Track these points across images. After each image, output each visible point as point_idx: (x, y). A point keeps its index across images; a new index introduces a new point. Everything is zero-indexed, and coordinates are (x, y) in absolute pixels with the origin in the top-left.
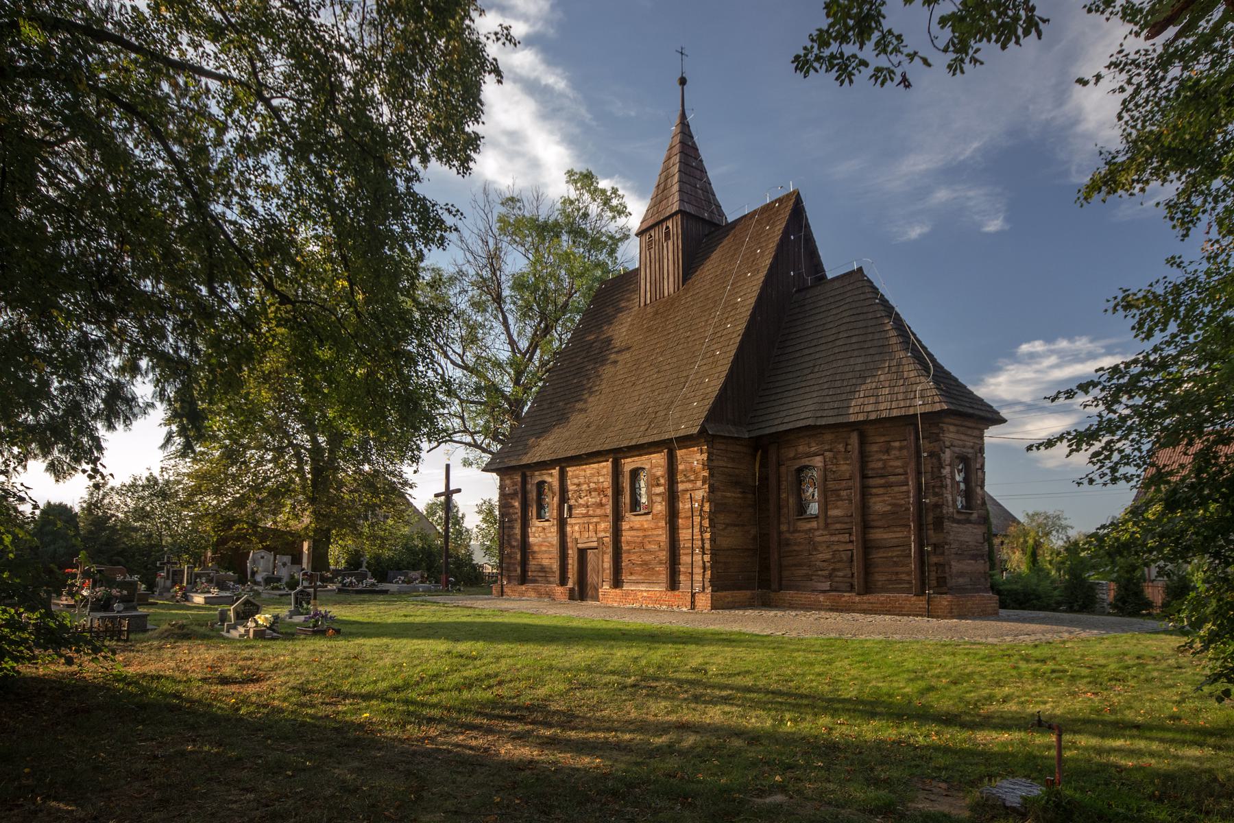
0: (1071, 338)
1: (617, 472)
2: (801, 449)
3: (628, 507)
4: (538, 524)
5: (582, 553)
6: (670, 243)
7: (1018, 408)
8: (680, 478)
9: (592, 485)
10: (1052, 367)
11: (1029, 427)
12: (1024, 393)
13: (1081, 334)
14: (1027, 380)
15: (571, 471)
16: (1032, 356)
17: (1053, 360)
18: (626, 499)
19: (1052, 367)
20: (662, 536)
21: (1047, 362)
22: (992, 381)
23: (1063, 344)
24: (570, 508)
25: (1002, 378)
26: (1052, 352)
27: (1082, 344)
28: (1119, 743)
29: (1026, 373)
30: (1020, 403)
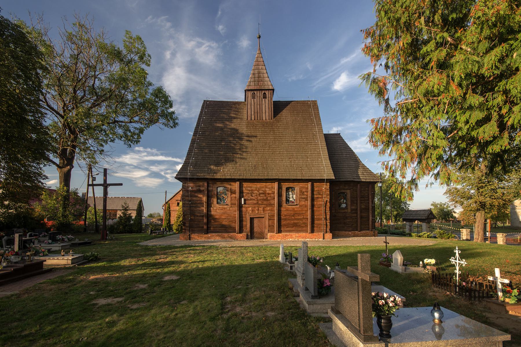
0: (151, 149)
1: (280, 188)
2: (341, 187)
3: (285, 202)
4: (218, 206)
5: (252, 219)
6: (255, 100)
7: (132, 167)
8: (315, 193)
9: (261, 192)
10: (145, 156)
11: (134, 173)
12: (134, 162)
13: (154, 148)
14: (135, 158)
15: (245, 185)
16: (139, 152)
17: (145, 154)
18: (284, 198)
19: (145, 156)
20: (237, 214)
21: (143, 154)
22: (124, 157)
23: (149, 150)
24: (245, 200)
25: (128, 156)
26: (146, 151)
27: (154, 151)
28: (138, 272)
29: (136, 156)
30: (132, 165)
